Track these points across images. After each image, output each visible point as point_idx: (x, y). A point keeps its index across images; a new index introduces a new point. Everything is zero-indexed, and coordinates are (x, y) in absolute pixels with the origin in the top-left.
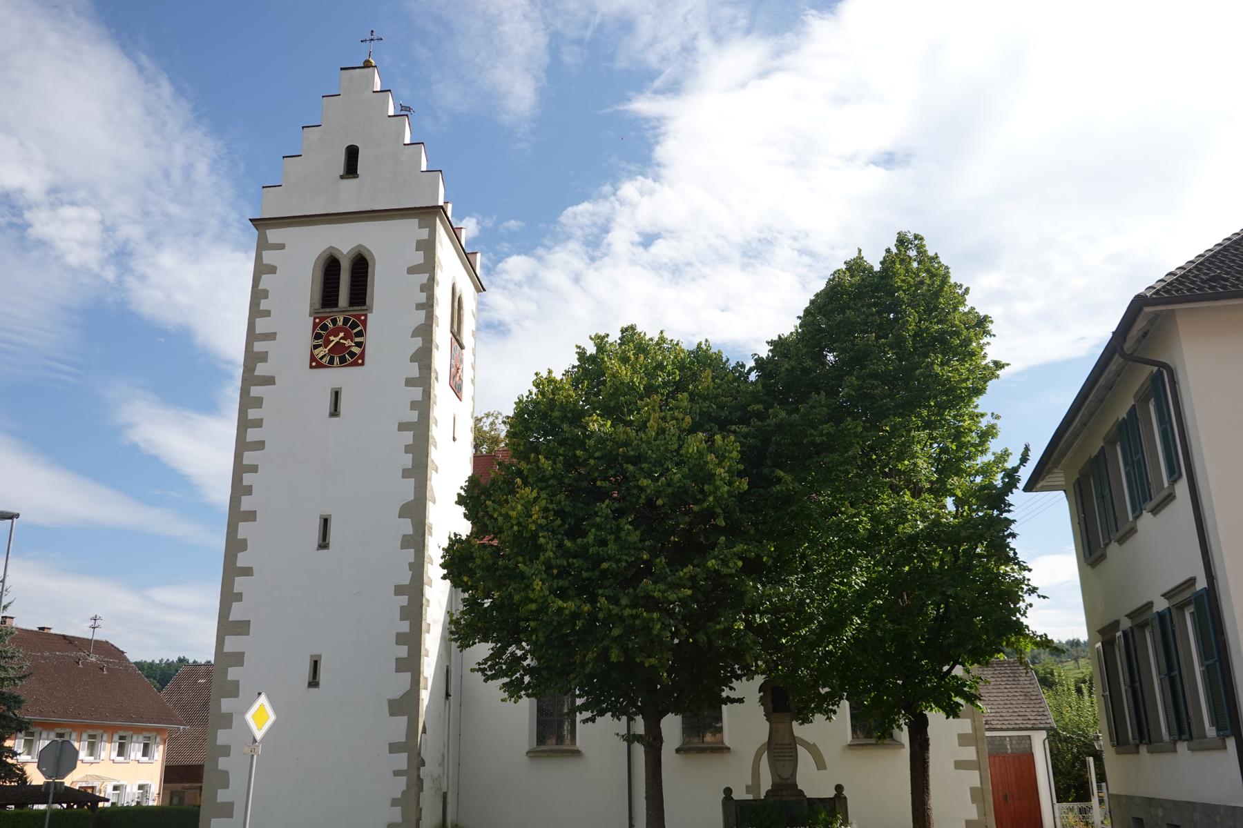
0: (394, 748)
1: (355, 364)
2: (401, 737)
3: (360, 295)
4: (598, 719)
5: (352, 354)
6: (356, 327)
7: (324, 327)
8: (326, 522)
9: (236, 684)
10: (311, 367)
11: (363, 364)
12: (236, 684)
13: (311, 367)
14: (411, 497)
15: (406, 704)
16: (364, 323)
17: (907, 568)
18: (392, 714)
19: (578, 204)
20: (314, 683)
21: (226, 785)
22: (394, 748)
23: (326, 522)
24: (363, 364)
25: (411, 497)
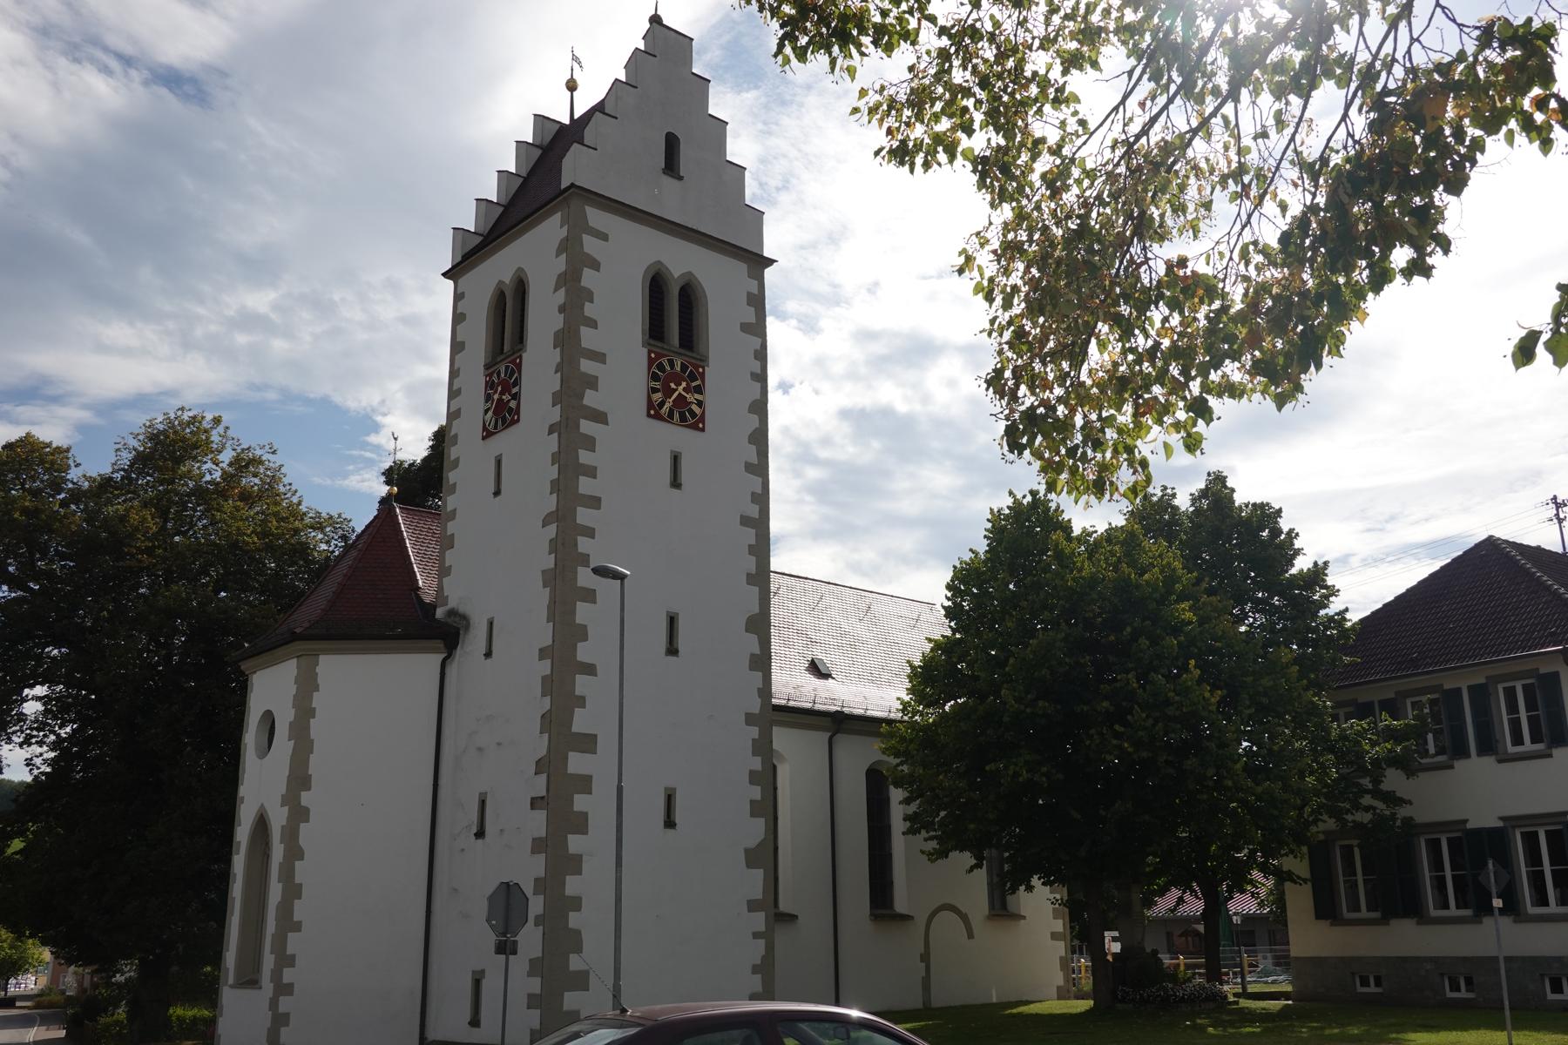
0: (753, 906)
1: (694, 427)
2: (758, 894)
3: (690, 337)
4: (1556, 752)
5: (693, 414)
6: (694, 376)
7: (661, 367)
8: (672, 621)
9: (584, 816)
10: (703, 430)
11: (649, 415)
12: (584, 816)
13: (703, 430)
14: (756, 609)
15: (765, 856)
16: (702, 375)
17: (17, 844)
18: (749, 866)
19: (1442, 568)
20: (670, 823)
21: (578, 949)
22: (753, 906)
23: (672, 621)
24: (649, 415)
25: (757, 610)
